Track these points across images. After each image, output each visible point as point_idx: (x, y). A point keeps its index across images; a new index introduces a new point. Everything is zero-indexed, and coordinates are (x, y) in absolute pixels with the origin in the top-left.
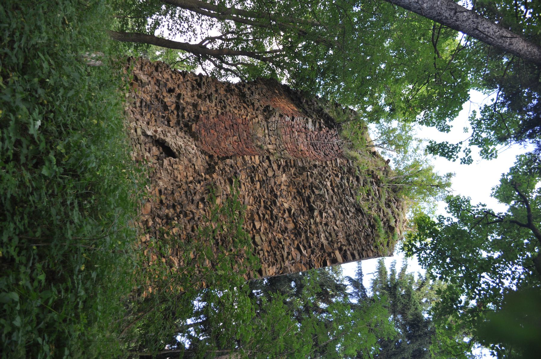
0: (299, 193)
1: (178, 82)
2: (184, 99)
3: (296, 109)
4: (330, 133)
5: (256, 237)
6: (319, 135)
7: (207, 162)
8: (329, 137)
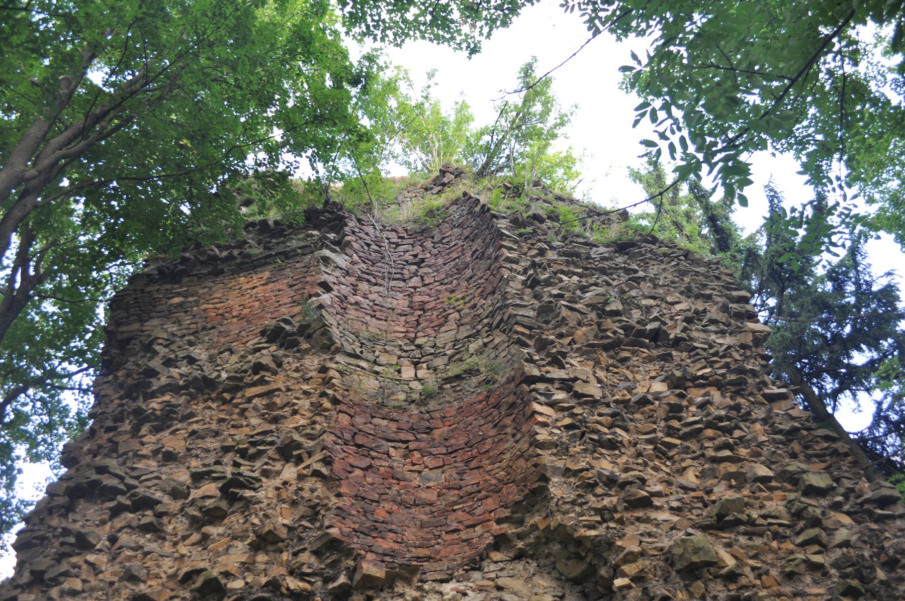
0: (612, 346)
1: (107, 576)
2: (227, 575)
3: (267, 274)
7: (512, 560)
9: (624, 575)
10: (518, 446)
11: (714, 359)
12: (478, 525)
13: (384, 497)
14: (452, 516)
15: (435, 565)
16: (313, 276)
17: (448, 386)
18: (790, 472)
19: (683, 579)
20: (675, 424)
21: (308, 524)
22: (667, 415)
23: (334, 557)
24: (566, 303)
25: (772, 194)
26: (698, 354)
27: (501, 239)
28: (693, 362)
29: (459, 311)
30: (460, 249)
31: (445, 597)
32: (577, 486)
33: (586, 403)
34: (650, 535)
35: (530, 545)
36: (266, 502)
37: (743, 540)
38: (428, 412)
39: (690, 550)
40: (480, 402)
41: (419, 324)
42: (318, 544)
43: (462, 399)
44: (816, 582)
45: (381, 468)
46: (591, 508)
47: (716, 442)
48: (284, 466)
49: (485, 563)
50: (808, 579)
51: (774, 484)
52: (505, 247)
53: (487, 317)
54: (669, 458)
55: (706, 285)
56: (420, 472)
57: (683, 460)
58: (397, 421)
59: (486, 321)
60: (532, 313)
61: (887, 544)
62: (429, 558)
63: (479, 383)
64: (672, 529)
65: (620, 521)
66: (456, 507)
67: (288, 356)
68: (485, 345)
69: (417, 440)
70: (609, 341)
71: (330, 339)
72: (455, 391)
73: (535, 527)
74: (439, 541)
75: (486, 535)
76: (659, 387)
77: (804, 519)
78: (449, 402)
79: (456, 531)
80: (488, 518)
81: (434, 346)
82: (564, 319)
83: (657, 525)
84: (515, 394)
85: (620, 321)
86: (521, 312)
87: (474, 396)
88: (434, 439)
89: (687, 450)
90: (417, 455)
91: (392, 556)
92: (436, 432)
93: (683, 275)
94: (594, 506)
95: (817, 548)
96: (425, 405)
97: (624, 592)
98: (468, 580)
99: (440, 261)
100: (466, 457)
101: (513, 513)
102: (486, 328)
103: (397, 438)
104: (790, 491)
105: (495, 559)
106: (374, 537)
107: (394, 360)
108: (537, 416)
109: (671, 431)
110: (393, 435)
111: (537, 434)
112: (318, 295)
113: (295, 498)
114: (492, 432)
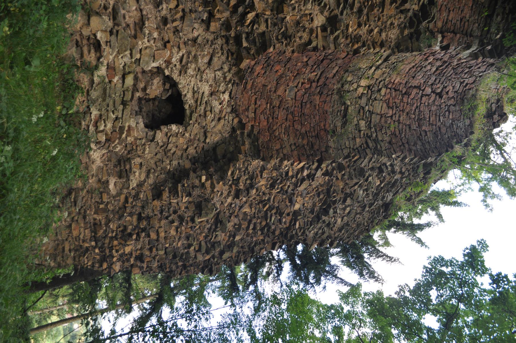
9: (207, 180)
10: (288, 146)
11: (302, 231)
12: (255, 115)
13: (287, 70)
14: (264, 102)
15: (240, 91)
16: (459, 39)
17: (343, 108)
18: (234, 247)
19: (198, 202)
20: (274, 211)
21: (282, 31)
22: (279, 209)
23: (258, 44)
24: (360, 183)
25: (393, 260)
26: (307, 225)
27: (420, 157)
28: (304, 222)
29: (392, 117)
30: (435, 123)
31: (222, 94)
32: (254, 173)
33: (297, 183)
34: (222, 194)
35: (237, 136)
36: (303, 9)
37: (208, 226)
38: (332, 94)
39: (208, 211)
40: (325, 126)
41: (396, 90)
42: (267, 38)
43: (332, 114)
44: (183, 244)
45: (305, 69)
46: (241, 176)
47: (258, 225)
48: (326, 17)
49: (234, 115)
50: (185, 242)
51: (231, 239)
52: (414, 158)
53: (376, 136)
54: (259, 203)
55: (347, 232)
56: (296, 87)
57: (256, 209)
58: (333, 78)
59: (374, 135)
60: (363, 165)
61: (192, 268)
62: (245, 88)
63: (336, 127)
64: (222, 202)
65: (231, 186)
66: (268, 105)
67: (405, 19)
68: (360, 131)
69: (317, 87)
70: (331, 193)
71: (402, 51)
72: (338, 111)
73: (244, 144)
74: (253, 94)
75: (248, 119)
76: (297, 207)
77: (211, 247)
78: (333, 107)
79: (256, 103)
80: (256, 121)
81: (375, 99)
82: (352, 179)
83: (225, 198)
84: (318, 150)
85: (340, 201)
86: (366, 160)
87: (330, 122)
88: (314, 95)
89: (260, 211)
90: (307, 86)
91: (250, 72)
92: (317, 98)
93: (357, 225)
94: (241, 178)
95: (197, 249)
96: (337, 93)
97: (199, 178)
98: (227, 106)
99: (434, 108)
100: (295, 113)
101: (254, 135)
102: (370, 134)
103: (322, 77)
104: (226, 243)
105: (235, 120)
106: (264, 64)
107: (376, 77)
108: (298, 162)
109: (271, 209)
110: (325, 75)
111: (288, 161)
112: (442, 42)
113: (301, 25)
114: (303, 130)
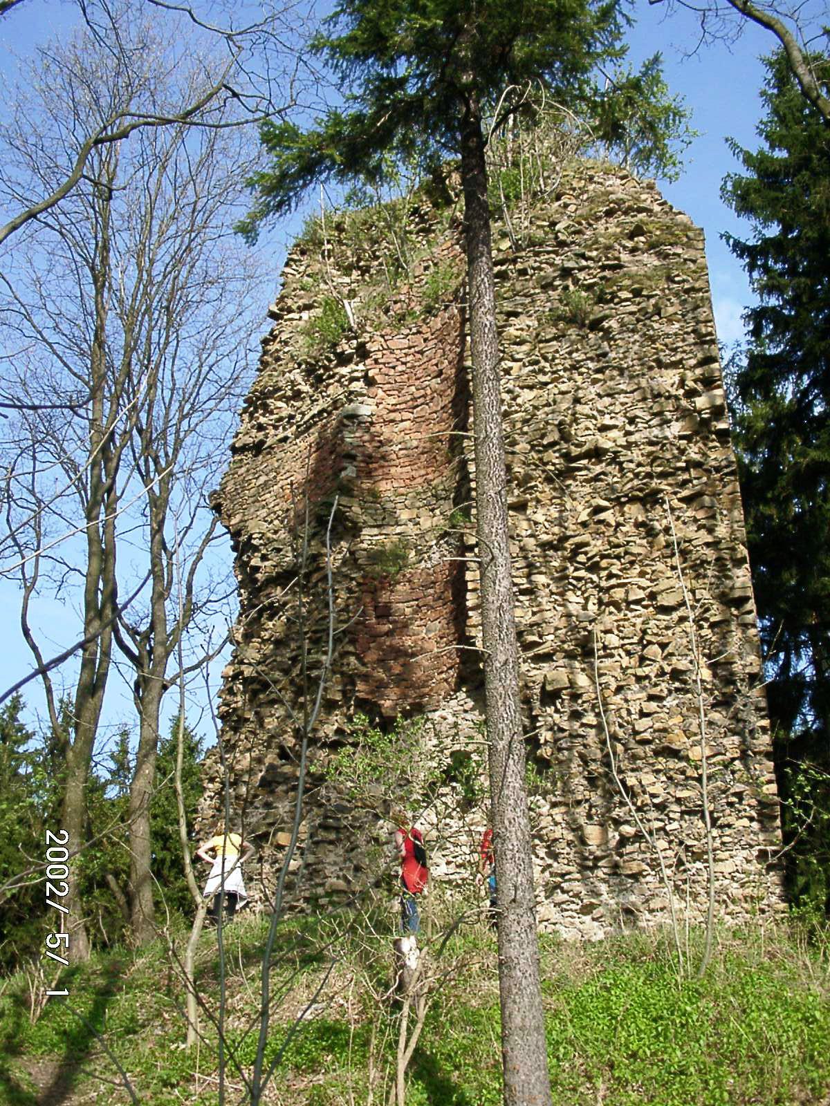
4: (379, 355)
5: (666, 604)
6: (386, 387)
8: (391, 359)
